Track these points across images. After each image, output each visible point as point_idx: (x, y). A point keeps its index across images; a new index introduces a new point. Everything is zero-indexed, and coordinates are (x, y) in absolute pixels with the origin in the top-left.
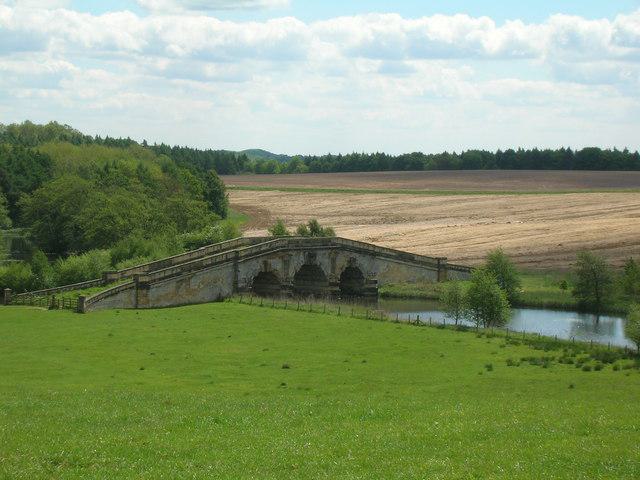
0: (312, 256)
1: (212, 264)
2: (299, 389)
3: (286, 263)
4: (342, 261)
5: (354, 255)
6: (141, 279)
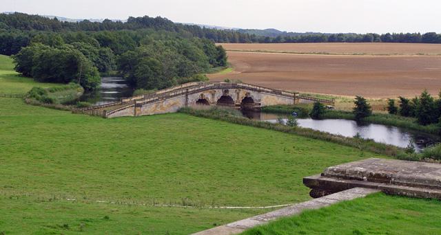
0: (226, 91)
1: (174, 96)
2: (5, 187)
3: (213, 95)
4: (242, 94)
5: (249, 91)
6: (137, 102)
